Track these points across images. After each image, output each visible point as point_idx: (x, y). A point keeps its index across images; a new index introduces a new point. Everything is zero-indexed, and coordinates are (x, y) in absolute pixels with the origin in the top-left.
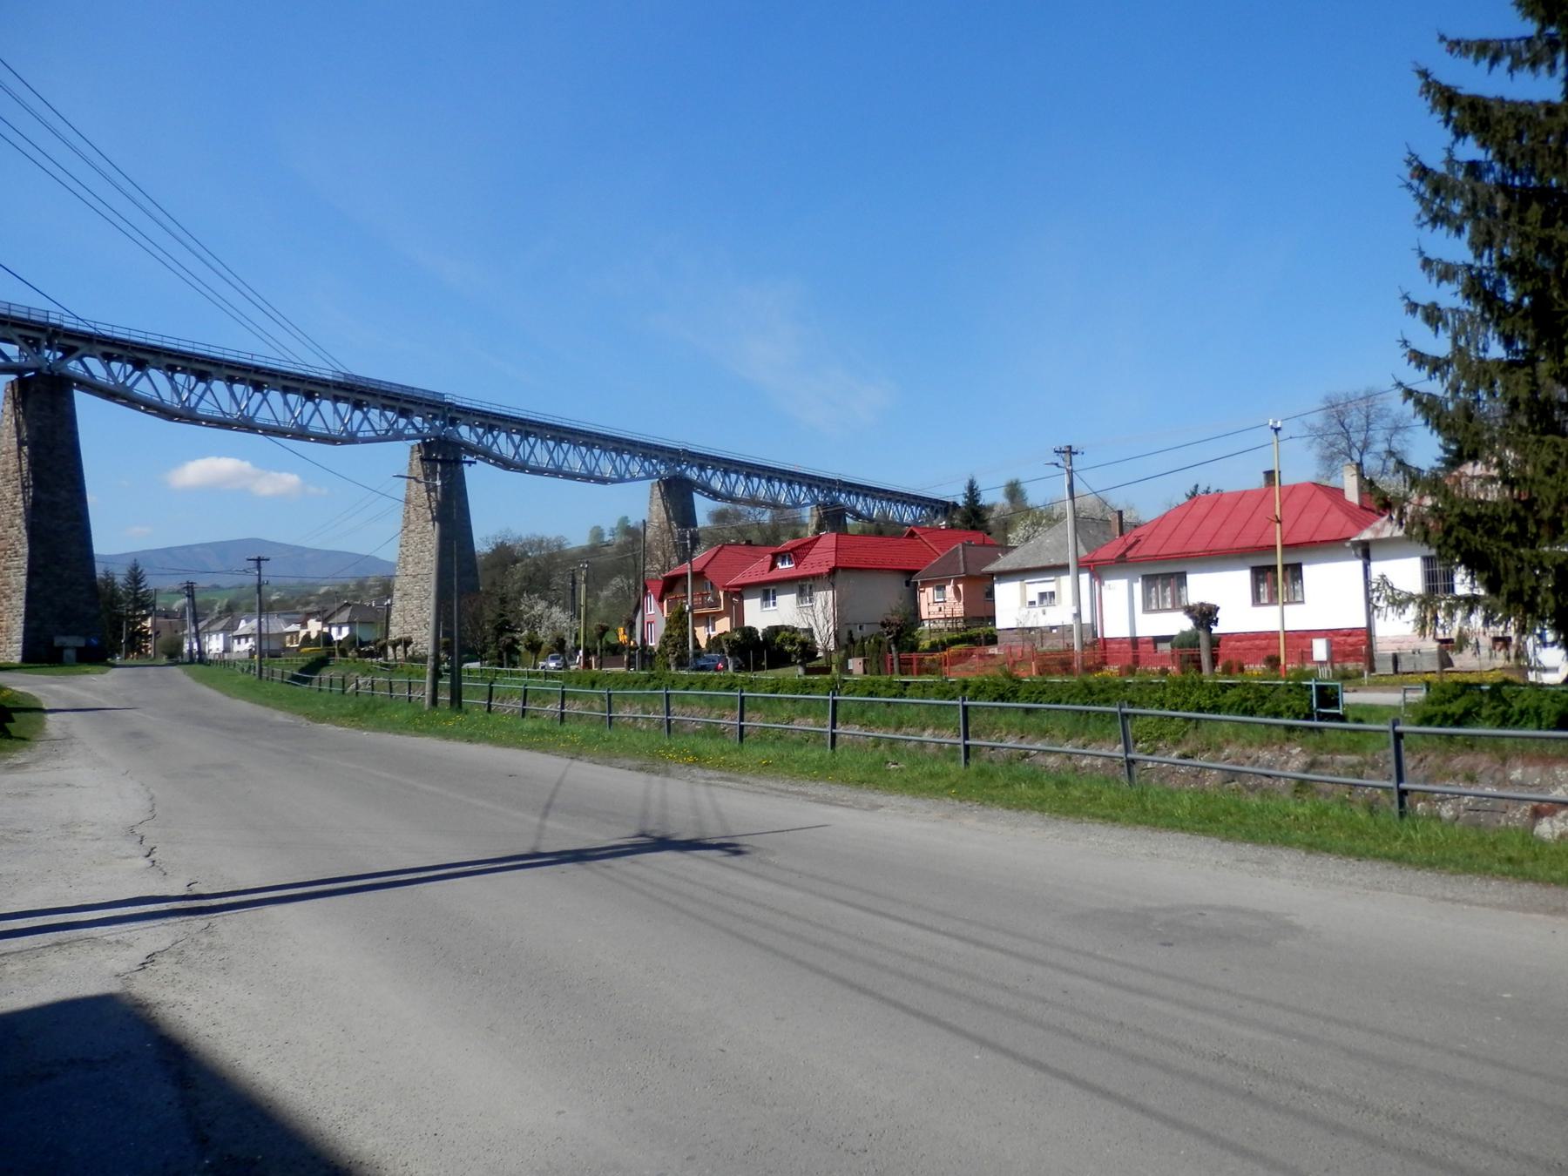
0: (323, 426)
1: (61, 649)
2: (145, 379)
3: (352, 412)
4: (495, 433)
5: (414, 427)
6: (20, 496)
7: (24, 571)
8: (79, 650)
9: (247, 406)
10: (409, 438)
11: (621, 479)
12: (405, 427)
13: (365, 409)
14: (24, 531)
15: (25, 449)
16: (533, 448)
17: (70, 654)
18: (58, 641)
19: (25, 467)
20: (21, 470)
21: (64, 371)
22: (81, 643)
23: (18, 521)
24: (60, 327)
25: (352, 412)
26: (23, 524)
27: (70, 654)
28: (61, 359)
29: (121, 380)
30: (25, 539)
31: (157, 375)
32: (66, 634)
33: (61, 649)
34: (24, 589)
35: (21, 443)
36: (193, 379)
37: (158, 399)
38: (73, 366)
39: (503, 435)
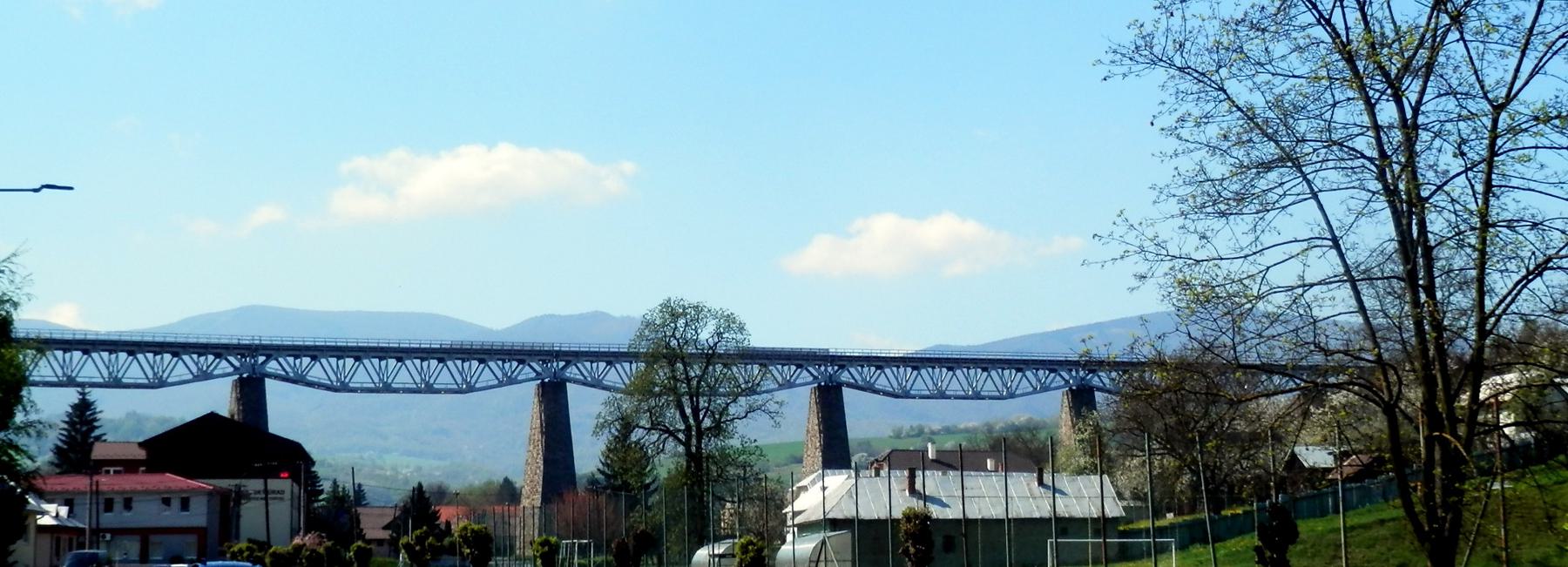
23: (538, 471)
30: (541, 483)
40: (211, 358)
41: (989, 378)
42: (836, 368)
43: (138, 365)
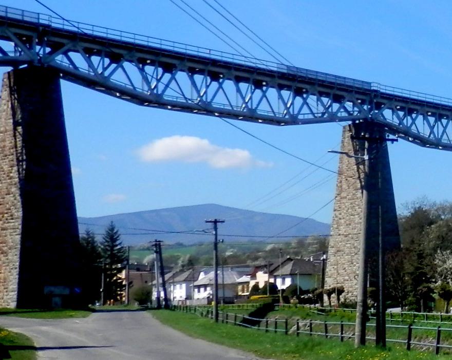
0: (270, 110)
3: (294, 98)
4: (414, 116)
5: (346, 110)
6: (15, 168)
9: (205, 93)
10: (342, 119)
12: (338, 111)
13: (305, 96)
14: (19, 198)
15: (20, 129)
19: (19, 144)
20: (16, 147)
22: (66, 292)
24: (49, 26)
25: (294, 98)
26: (18, 192)
28: (50, 53)
30: (19, 204)
35: (16, 124)
37: (131, 87)
39: (421, 117)
40: (107, 61)
42: (48, 50)
43: (223, 92)
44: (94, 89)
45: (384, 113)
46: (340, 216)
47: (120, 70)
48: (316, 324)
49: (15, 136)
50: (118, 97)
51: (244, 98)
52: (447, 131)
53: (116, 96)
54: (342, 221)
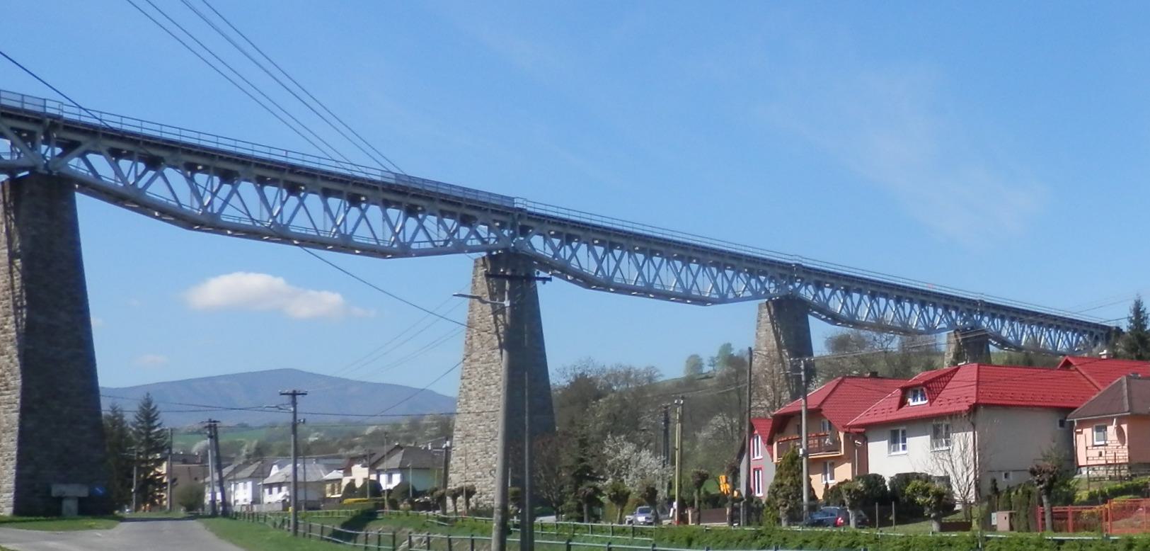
1: (60, 499)
2: (159, 179)
3: (405, 220)
4: (574, 244)
5: (479, 237)
6: (12, 318)
7: (17, 407)
8: (81, 500)
10: (473, 250)
11: (723, 300)
12: (468, 237)
14: (16, 360)
15: (18, 262)
16: (618, 262)
17: (70, 505)
18: (56, 490)
19: (17, 283)
20: (12, 287)
21: (64, 171)
22: (84, 492)
25: (405, 220)
27: (70, 505)
28: (61, 155)
29: (131, 180)
30: (17, 369)
31: (174, 175)
32: (65, 482)
33: (60, 499)
34: (17, 428)
36: (217, 180)
38: (75, 164)
39: (584, 247)
41: (363, 221)
43: (305, 213)
44: (122, 206)
45: (532, 240)
46: (470, 386)
47: (159, 179)
48: (436, 539)
49: (11, 272)
50: (157, 218)
51: (334, 220)
52: (578, 254)
53: (567, 280)
54: (473, 393)
